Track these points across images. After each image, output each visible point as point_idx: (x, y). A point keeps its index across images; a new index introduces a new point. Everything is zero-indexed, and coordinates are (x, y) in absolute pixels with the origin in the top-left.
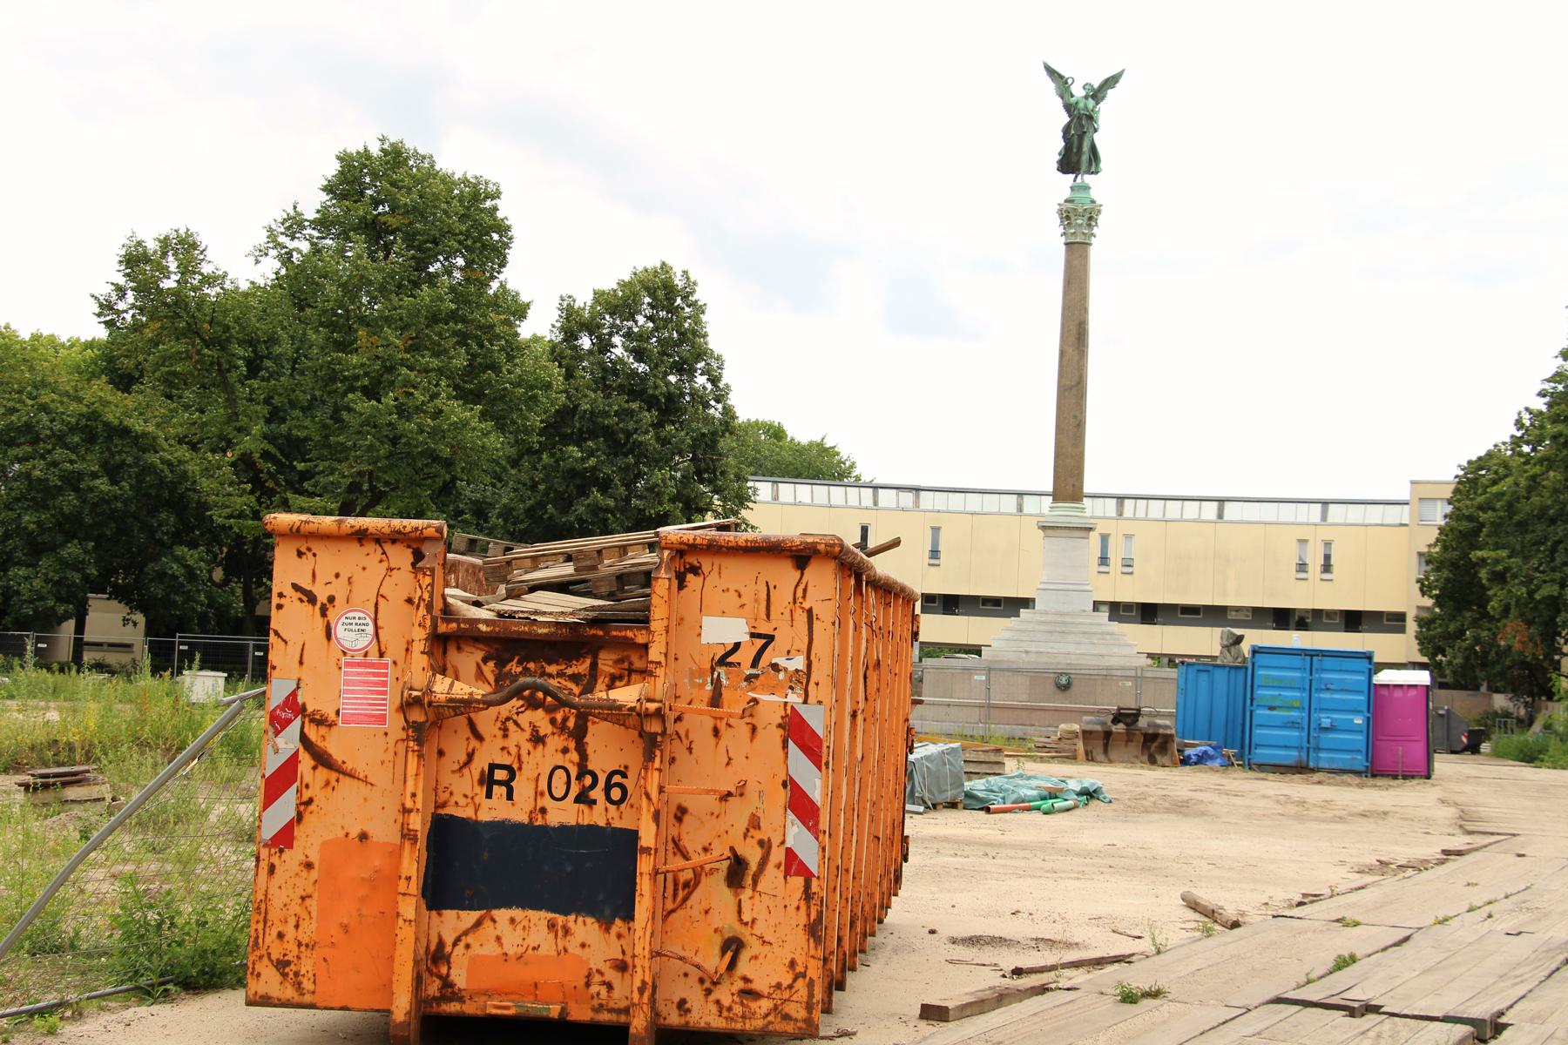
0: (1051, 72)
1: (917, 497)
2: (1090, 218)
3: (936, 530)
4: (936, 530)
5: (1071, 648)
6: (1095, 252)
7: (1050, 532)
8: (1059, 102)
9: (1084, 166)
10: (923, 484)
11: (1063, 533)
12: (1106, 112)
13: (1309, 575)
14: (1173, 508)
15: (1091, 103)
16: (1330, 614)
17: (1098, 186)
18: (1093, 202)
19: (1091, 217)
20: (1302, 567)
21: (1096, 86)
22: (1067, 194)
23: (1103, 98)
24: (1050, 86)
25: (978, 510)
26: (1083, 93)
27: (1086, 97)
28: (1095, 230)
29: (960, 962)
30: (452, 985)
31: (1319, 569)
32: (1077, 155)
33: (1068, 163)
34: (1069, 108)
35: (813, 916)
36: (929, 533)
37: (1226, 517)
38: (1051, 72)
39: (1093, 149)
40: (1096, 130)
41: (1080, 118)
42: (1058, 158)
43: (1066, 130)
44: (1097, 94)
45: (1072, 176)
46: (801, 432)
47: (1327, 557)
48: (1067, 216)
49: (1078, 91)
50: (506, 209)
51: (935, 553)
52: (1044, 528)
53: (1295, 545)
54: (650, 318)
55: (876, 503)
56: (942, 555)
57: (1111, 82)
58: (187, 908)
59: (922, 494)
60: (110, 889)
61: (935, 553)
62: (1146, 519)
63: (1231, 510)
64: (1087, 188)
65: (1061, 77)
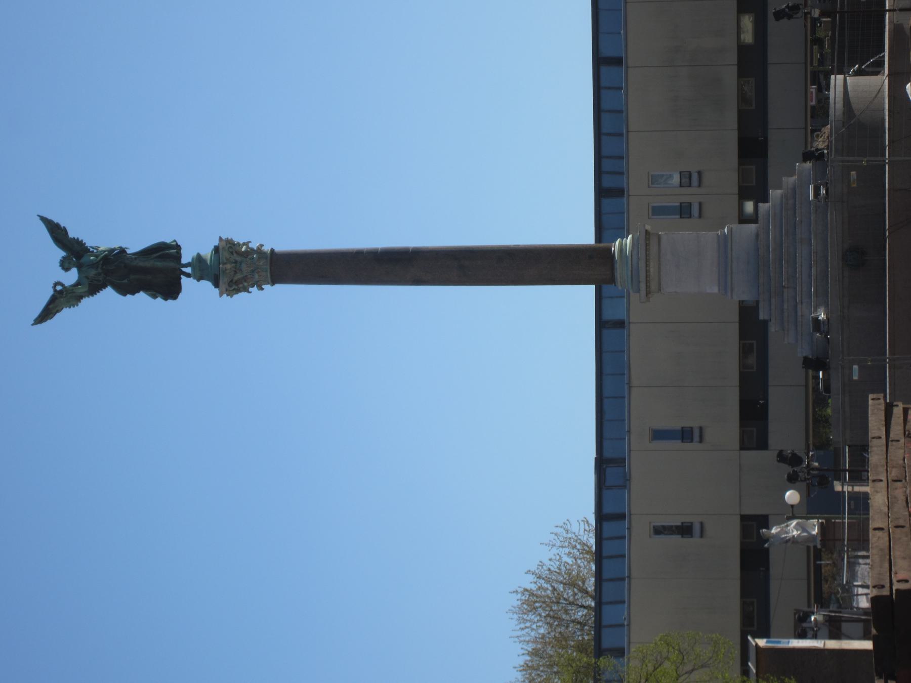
0: (47, 314)
3: (658, 435)
4: (658, 435)
6: (282, 246)
8: (86, 302)
9: (172, 264)
12: (100, 238)
17: (196, 245)
21: (62, 254)
24: (66, 314)
29: (660, 284)
32: (154, 272)
34: (94, 289)
38: (47, 314)
39: (147, 253)
44: (74, 251)
45: (184, 279)
49: (71, 277)
50: (170, 301)
51: (685, 435)
56: (687, 424)
57: (57, 233)
58: (542, 631)
61: (685, 435)
64: (199, 259)
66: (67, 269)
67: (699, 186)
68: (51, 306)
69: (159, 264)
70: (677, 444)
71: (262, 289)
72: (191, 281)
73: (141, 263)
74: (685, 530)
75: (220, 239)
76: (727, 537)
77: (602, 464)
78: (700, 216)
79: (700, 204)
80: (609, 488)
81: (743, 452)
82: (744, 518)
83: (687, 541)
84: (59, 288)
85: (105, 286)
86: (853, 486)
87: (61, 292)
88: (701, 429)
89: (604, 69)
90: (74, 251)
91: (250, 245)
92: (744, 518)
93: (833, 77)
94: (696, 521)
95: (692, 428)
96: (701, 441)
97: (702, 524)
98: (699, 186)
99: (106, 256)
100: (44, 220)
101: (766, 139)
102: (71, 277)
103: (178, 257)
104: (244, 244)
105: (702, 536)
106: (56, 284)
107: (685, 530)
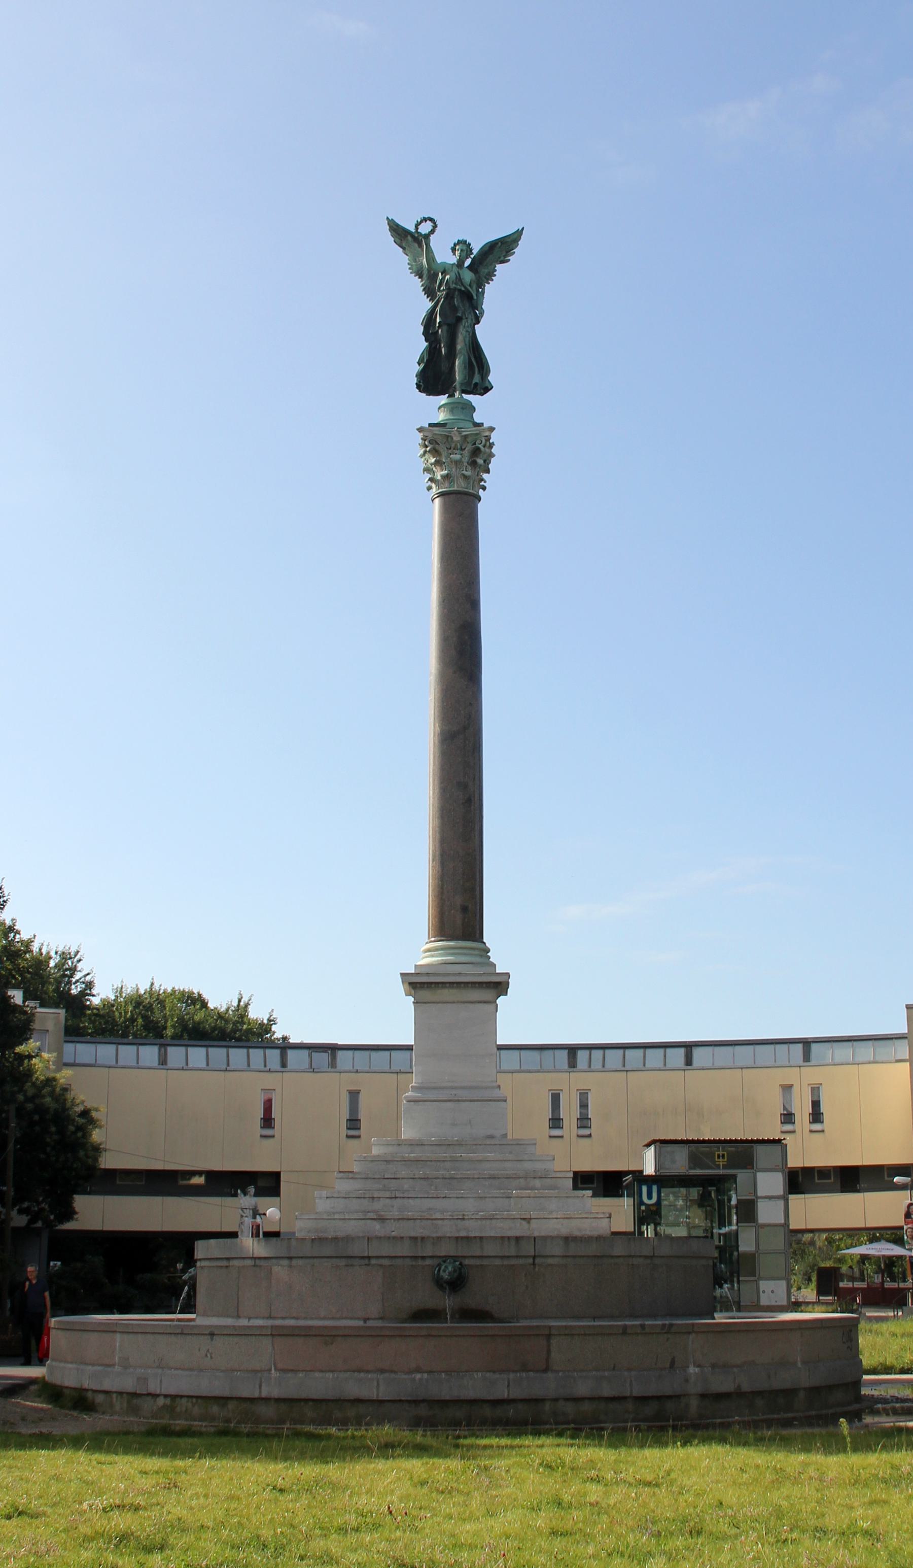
1: (334, 1058)
2: (476, 452)
3: (354, 1095)
4: (354, 1095)
5: (469, 1206)
6: (484, 510)
7: (425, 994)
12: (495, 296)
16: (823, 1172)
30: (703, 1201)
31: (806, 1118)
32: (451, 362)
33: (433, 379)
36: (345, 1098)
39: (475, 350)
42: (417, 368)
43: (429, 322)
46: (219, 999)
47: (816, 1104)
51: (354, 1123)
53: (778, 1091)
54: (908, 1490)
57: (501, 249)
59: (340, 1054)
61: (354, 1123)
67: (578, 1136)
68: (409, 238)
70: (346, 1115)
74: (268, 1121)
75: (492, 429)
76: (260, 1161)
77: (332, 1049)
78: (551, 1137)
79: (562, 1137)
80: (310, 1056)
81: (278, 1170)
82: (277, 1175)
83: (258, 1123)
88: (359, 1137)
89: (682, 1051)
92: (277, 1175)
93: (865, 1391)
94: (276, 1131)
95: (359, 1129)
96: (348, 1137)
97: (273, 1136)
98: (578, 1136)
100: (518, 234)
101: (858, 1191)
102: (444, 255)
105: (262, 1136)
107: (268, 1121)
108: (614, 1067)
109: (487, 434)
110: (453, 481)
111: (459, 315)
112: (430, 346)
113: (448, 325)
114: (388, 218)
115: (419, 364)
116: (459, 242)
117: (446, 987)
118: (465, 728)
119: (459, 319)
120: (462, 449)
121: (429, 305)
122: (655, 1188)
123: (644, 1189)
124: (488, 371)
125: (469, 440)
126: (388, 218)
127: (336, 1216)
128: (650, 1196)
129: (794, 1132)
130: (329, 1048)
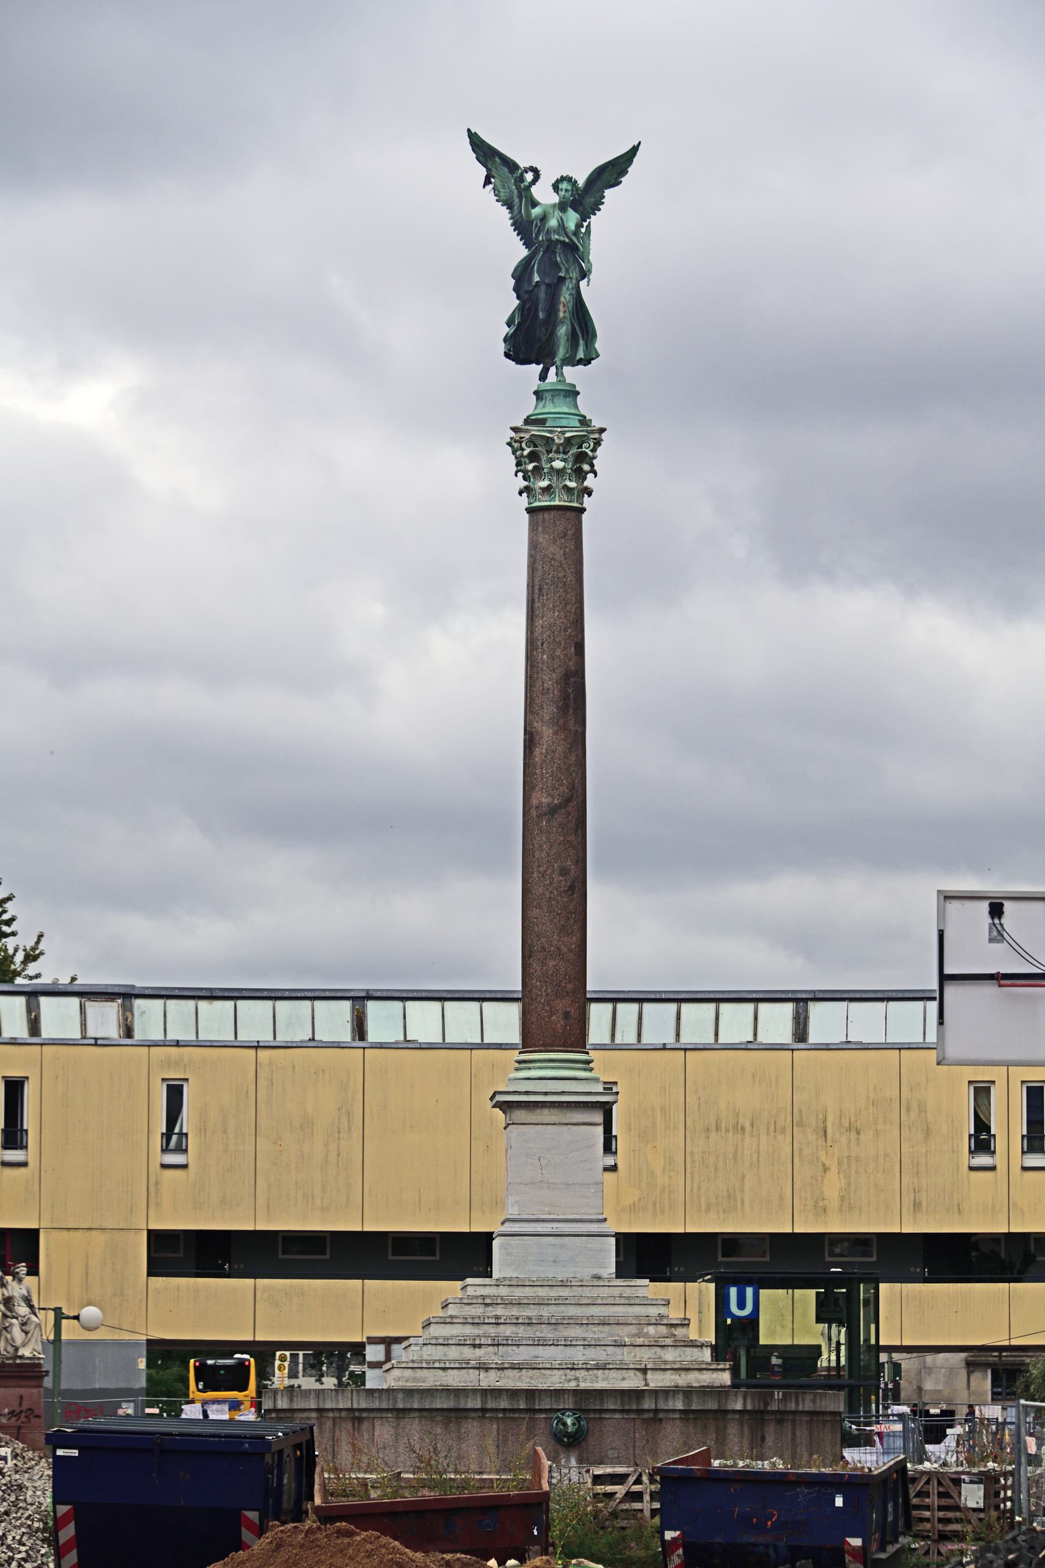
1: (127, 1010)
9: (561, 353)
10: (140, 983)
11: (546, 1115)
13: (999, 1159)
14: (697, 1019)
15: (572, 218)
17: (595, 388)
18: (584, 422)
19: (581, 452)
20: (982, 1140)
22: (529, 406)
23: (595, 207)
25: (267, 1037)
26: (555, 199)
27: (562, 206)
28: (590, 481)
31: (1017, 1144)
34: (523, 227)
35: (895, 1418)
37: (813, 1038)
40: (584, 274)
41: (551, 247)
42: (505, 330)
43: (522, 274)
44: (585, 197)
45: (536, 369)
48: (531, 450)
49: (544, 194)
50: (502, 347)
52: (506, 1107)
55: (34, 1028)
57: (612, 172)
60: (779, 1361)
62: (639, 1047)
63: (826, 1022)
65: (511, 166)
66: (556, 187)
68: (497, 159)
69: (562, 331)
71: (521, 493)
72: (535, 384)
73: (566, 296)
83: (965, 1145)
84: (529, 177)
85: (527, 244)
86: (231, 1420)
87: (521, 179)
90: (585, 197)
91: (590, 476)
99: (577, 248)
100: (634, 150)
103: (572, 361)
104: (592, 466)
106: (536, 172)
108: (659, 1041)
109: (596, 436)
110: (554, 492)
111: (562, 274)
112: (521, 308)
113: (548, 285)
114: (469, 130)
115: (509, 326)
116: (563, 179)
117: (546, 1107)
118: (568, 801)
119: (562, 280)
120: (565, 453)
121: (524, 252)
122: (749, 1291)
123: (733, 1291)
124: (594, 335)
125: (573, 441)
126: (469, 130)
127: (437, 1365)
128: (741, 1305)
129: (993, 1168)
130: (119, 995)
